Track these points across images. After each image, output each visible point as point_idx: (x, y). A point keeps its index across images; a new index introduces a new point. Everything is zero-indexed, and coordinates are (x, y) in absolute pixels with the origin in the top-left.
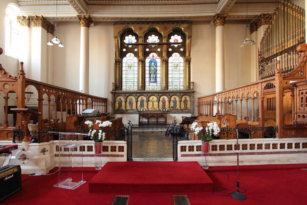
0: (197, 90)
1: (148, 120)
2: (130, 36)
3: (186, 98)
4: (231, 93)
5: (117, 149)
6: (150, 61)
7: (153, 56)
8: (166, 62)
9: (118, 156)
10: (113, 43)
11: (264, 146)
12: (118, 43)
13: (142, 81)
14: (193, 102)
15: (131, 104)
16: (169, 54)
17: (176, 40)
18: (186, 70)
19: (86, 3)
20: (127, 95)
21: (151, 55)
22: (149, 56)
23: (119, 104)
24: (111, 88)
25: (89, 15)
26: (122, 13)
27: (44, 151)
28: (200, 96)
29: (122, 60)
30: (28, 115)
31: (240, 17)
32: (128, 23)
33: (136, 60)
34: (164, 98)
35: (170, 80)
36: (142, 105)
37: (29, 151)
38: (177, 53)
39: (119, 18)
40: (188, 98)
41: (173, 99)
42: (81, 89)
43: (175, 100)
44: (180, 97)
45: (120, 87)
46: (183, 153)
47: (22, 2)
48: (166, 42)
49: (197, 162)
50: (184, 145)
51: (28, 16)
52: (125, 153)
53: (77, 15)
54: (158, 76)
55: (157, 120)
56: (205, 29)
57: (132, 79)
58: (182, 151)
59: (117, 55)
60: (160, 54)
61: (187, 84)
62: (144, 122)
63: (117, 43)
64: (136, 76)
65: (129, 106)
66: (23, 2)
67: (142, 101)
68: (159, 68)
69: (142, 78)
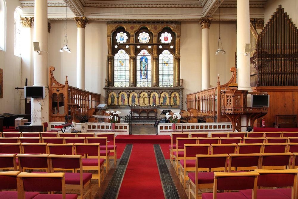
0: (186, 87)
1: (140, 115)
2: (122, 32)
3: (175, 95)
4: (200, 94)
5: (123, 127)
6: (141, 58)
7: (144, 53)
8: (156, 60)
9: (124, 131)
10: (106, 41)
11: (208, 127)
12: (111, 41)
13: (133, 77)
14: (182, 99)
15: (123, 99)
16: (160, 52)
17: (166, 37)
18: (176, 67)
19: (83, 5)
20: (119, 91)
21: (142, 51)
22: (140, 53)
23: (111, 99)
24: (104, 84)
25: (86, 17)
26: (115, 15)
27: (83, 128)
28: (189, 93)
29: (114, 57)
30: (75, 107)
31: (224, 20)
32: (121, 22)
33: (127, 56)
34: (154, 95)
35: (160, 77)
36: (133, 101)
37: (75, 127)
38: (167, 50)
39: (112, 19)
40: (177, 95)
41: (163, 96)
42: (78, 86)
43: (165, 96)
44: (170, 93)
45: (112, 83)
46: (162, 130)
47: (25, 4)
48: (156, 43)
49: (169, 135)
50: (162, 126)
51: (31, 18)
52: (128, 130)
53: (75, 17)
54: (149, 72)
55: (148, 115)
56: (194, 27)
57: (124, 75)
58: (161, 129)
59: (110, 52)
60: (151, 52)
61: (177, 81)
62: (136, 117)
63: (110, 40)
64: (128, 72)
65: (121, 101)
66: (25, 5)
67: (134, 97)
68: (149, 65)
69: (133, 74)
